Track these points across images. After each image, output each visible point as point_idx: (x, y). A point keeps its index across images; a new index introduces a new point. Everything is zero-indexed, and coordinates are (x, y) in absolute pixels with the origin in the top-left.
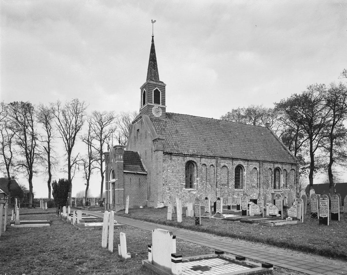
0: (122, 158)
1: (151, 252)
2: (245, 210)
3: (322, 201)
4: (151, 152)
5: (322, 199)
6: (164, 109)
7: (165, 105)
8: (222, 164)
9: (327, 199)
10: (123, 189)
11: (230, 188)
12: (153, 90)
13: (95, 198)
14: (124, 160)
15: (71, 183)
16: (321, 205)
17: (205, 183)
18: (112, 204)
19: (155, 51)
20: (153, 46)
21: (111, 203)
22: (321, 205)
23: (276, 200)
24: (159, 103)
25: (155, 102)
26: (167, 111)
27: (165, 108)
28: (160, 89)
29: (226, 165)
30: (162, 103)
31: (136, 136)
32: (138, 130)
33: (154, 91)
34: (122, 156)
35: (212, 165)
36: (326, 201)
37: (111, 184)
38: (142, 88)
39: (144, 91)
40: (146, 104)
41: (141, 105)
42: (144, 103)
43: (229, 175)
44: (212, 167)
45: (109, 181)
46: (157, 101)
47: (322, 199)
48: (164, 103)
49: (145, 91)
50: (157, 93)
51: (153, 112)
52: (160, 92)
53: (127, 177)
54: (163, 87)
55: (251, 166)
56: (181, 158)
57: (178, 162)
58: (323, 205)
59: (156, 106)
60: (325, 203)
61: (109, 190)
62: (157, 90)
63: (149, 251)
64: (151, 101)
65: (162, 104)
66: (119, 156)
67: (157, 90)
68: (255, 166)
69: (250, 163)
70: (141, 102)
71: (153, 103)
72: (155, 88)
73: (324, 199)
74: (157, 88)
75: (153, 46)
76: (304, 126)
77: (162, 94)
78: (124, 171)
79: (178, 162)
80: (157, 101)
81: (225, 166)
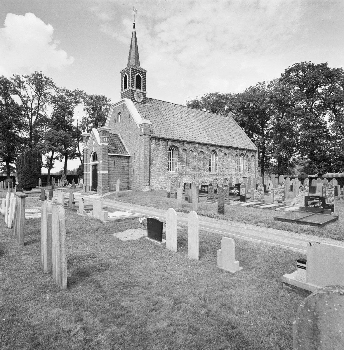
0: (106, 141)
1: (306, 269)
2: (244, 195)
3: (329, 190)
4: (136, 136)
5: (328, 188)
6: (145, 95)
7: (145, 91)
8: (200, 150)
9: (333, 188)
10: (107, 172)
11: (205, 171)
12: (134, 75)
16: (328, 193)
18: (92, 187)
21: (91, 185)
22: (328, 193)
24: (141, 89)
25: (137, 87)
27: (146, 94)
28: (141, 75)
29: (203, 150)
30: (143, 88)
31: (116, 119)
32: (119, 113)
33: (136, 76)
35: (191, 150)
36: (333, 190)
37: (91, 166)
38: (123, 73)
39: (126, 75)
41: (122, 89)
43: (205, 159)
44: (191, 152)
45: (89, 163)
47: (328, 188)
48: (145, 89)
49: (127, 75)
51: (135, 96)
53: (112, 160)
54: (144, 73)
55: (222, 152)
56: (165, 143)
57: (163, 146)
58: (329, 194)
59: (138, 91)
60: (332, 192)
61: (89, 172)
63: (298, 267)
65: (143, 90)
66: (104, 138)
67: (138, 75)
68: (225, 152)
69: (221, 149)
70: (122, 86)
72: (136, 74)
73: (330, 189)
74: (138, 74)
77: (143, 79)
79: (163, 146)
80: (139, 86)
81: (202, 152)
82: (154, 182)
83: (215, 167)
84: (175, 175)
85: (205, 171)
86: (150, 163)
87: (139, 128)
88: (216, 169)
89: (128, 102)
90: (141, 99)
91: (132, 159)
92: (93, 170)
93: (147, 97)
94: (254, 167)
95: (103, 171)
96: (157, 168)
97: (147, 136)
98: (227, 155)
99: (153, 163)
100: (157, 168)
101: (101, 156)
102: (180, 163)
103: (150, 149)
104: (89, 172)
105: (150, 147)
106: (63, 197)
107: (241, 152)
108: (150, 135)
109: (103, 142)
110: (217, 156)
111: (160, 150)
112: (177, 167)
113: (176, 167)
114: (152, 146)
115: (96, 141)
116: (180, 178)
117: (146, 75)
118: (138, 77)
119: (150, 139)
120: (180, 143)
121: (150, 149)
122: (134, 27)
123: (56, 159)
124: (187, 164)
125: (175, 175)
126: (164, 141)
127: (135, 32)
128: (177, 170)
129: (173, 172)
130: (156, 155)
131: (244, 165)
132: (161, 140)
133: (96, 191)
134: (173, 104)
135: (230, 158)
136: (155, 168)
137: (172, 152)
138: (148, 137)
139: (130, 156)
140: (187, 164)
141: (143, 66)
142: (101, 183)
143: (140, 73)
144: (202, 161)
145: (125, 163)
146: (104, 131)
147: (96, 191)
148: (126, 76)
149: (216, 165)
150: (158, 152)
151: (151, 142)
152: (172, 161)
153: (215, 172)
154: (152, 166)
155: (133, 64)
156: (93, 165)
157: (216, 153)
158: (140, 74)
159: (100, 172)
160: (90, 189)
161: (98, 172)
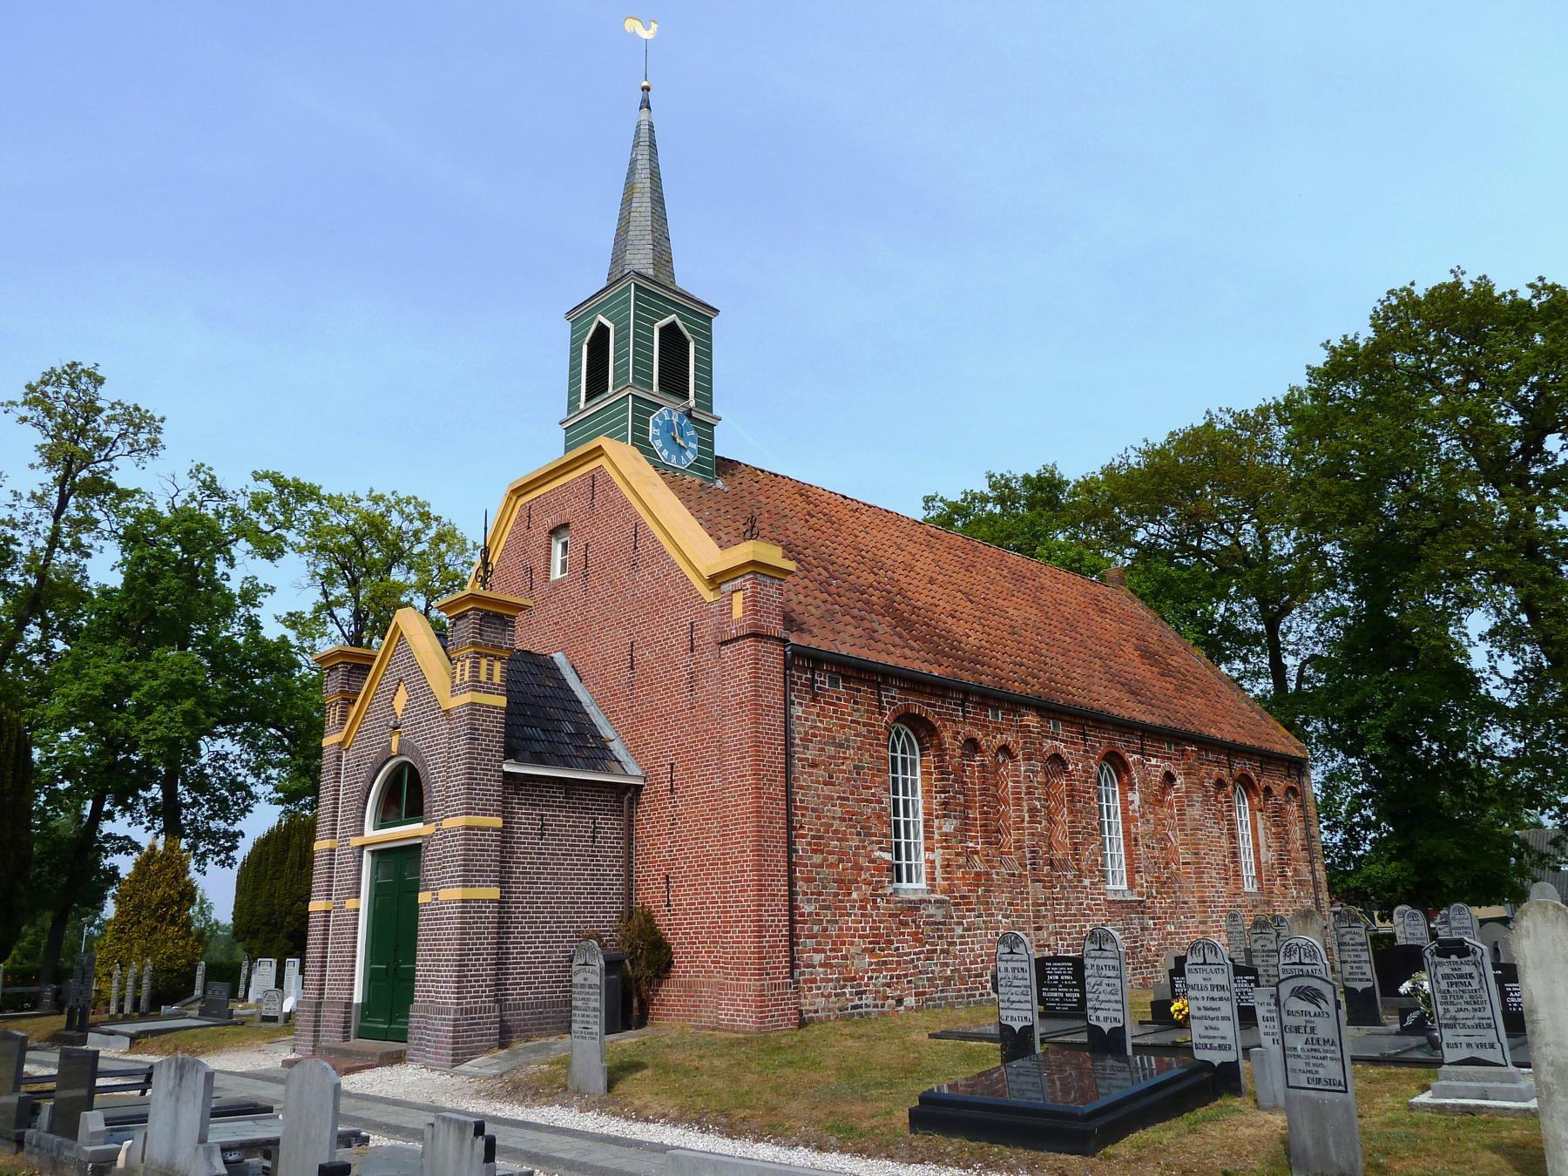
0: (497, 679)
7: (710, 409)
13: (362, 1021)
14: (508, 693)
15: (235, 907)
17: (977, 852)
19: (670, 261)
20: (648, 141)
21: (358, 998)
23: (1088, 962)
26: (721, 450)
33: (662, 330)
34: (498, 666)
38: (577, 316)
40: (610, 390)
41: (572, 405)
42: (597, 385)
45: (356, 842)
46: (674, 382)
48: (706, 400)
50: (673, 341)
51: (655, 438)
52: (608, 330)
54: (702, 315)
55: (1154, 761)
62: (673, 324)
64: (643, 308)
66: (484, 662)
67: (673, 324)
71: (656, 388)
75: (648, 141)
76: (1262, 537)
78: (506, 768)
82: (818, 958)
83: (1129, 854)
84: (932, 910)
85: (1087, 882)
86: (790, 827)
87: (709, 596)
88: (1133, 871)
89: (622, 458)
90: (688, 453)
91: (645, 815)
92: (378, 891)
93: (716, 454)
94: (1304, 854)
95: (466, 883)
96: (832, 859)
97: (770, 646)
98: (1180, 781)
99: (808, 825)
100: (832, 859)
101: (458, 784)
102: (949, 826)
103: (788, 733)
104: (350, 904)
105: (788, 717)
106: (335, 1126)
107: (1239, 766)
108: (785, 641)
109: (476, 686)
110: (1131, 785)
111: (840, 737)
112: (938, 856)
113: (932, 856)
114: (797, 711)
115: (421, 691)
116: (959, 931)
117: (709, 329)
118: (670, 332)
119: (788, 665)
120: (943, 697)
121: (788, 733)
122: (646, 104)
123: (308, 612)
124: (992, 834)
125: (932, 910)
126: (862, 681)
127: (651, 126)
128: (938, 873)
129: (914, 885)
130: (820, 772)
131: (1256, 846)
132: (846, 679)
133: (402, 1037)
134: (847, 501)
135: (1197, 797)
136: (817, 859)
137: (899, 755)
138: (773, 657)
139: (639, 788)
140: (992, 834)
141: (690, 277)
142: (449, 972)
143: (682, 318)
144: (1064, 816)
145: (610, 826)
146: (487, 614)
147: (402, 1037)
148: (602, 331)
149: (1131, 841)
150: (831, 750)
151: (788, 685)
152: (906, 814)
153: (1131, 885)
154: (800, 845)
155: (641, 260)
156: (383, 855)
157: (1127, 769)
158: (679, 323)
159: (444, 894)
160: (347, 1026)
161: (424, 897)
